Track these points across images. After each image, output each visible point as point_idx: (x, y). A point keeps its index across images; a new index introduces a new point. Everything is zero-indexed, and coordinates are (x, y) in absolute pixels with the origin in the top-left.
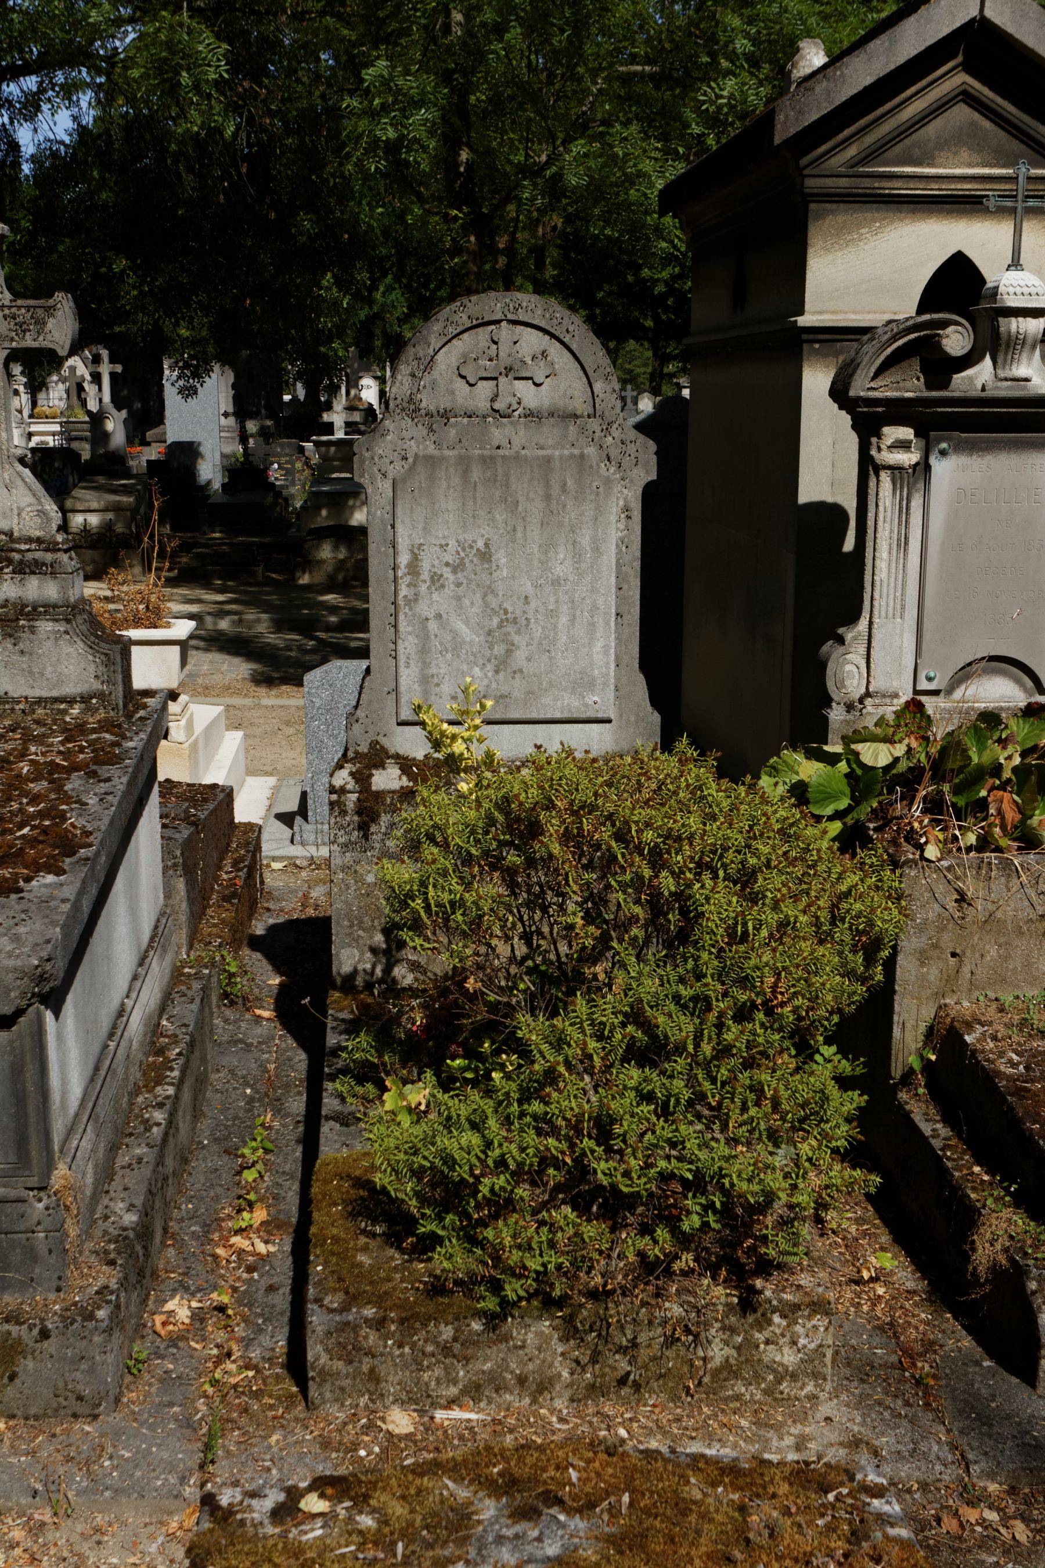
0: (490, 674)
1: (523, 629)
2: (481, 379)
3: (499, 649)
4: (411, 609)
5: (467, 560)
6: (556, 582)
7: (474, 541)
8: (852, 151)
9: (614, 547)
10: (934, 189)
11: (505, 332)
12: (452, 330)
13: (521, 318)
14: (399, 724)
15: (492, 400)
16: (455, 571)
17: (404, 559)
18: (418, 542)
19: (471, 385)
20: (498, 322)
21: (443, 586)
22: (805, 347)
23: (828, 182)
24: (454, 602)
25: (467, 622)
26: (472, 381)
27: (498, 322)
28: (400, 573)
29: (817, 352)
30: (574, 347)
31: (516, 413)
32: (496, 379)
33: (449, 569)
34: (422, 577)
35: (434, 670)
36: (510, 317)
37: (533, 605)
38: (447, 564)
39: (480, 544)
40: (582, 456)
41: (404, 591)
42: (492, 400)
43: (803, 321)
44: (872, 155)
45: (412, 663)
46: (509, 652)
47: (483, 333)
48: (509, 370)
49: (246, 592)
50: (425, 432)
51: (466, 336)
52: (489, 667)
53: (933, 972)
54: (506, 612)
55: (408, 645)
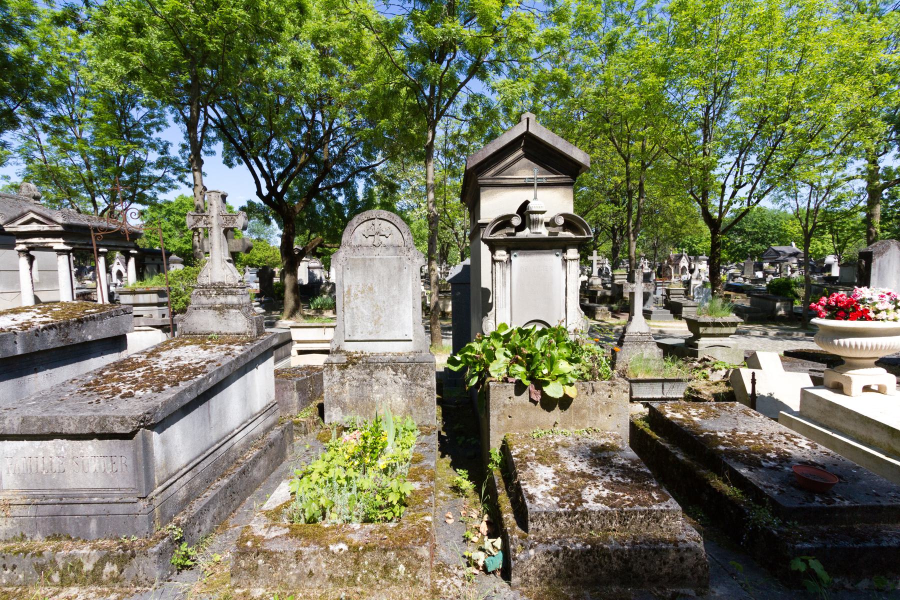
3: (376, 318)
6: (393, 297)
8: (492, 172)
10: (518, 182)
11: (376, 222)
17: (346, 289)
43: (479, 221)
44: (500, 172)
46: (379, 319)
47: (370, 222)
48: (377, 233)
49: (784, 329)
53: (503, 423)
55: (347, 316)
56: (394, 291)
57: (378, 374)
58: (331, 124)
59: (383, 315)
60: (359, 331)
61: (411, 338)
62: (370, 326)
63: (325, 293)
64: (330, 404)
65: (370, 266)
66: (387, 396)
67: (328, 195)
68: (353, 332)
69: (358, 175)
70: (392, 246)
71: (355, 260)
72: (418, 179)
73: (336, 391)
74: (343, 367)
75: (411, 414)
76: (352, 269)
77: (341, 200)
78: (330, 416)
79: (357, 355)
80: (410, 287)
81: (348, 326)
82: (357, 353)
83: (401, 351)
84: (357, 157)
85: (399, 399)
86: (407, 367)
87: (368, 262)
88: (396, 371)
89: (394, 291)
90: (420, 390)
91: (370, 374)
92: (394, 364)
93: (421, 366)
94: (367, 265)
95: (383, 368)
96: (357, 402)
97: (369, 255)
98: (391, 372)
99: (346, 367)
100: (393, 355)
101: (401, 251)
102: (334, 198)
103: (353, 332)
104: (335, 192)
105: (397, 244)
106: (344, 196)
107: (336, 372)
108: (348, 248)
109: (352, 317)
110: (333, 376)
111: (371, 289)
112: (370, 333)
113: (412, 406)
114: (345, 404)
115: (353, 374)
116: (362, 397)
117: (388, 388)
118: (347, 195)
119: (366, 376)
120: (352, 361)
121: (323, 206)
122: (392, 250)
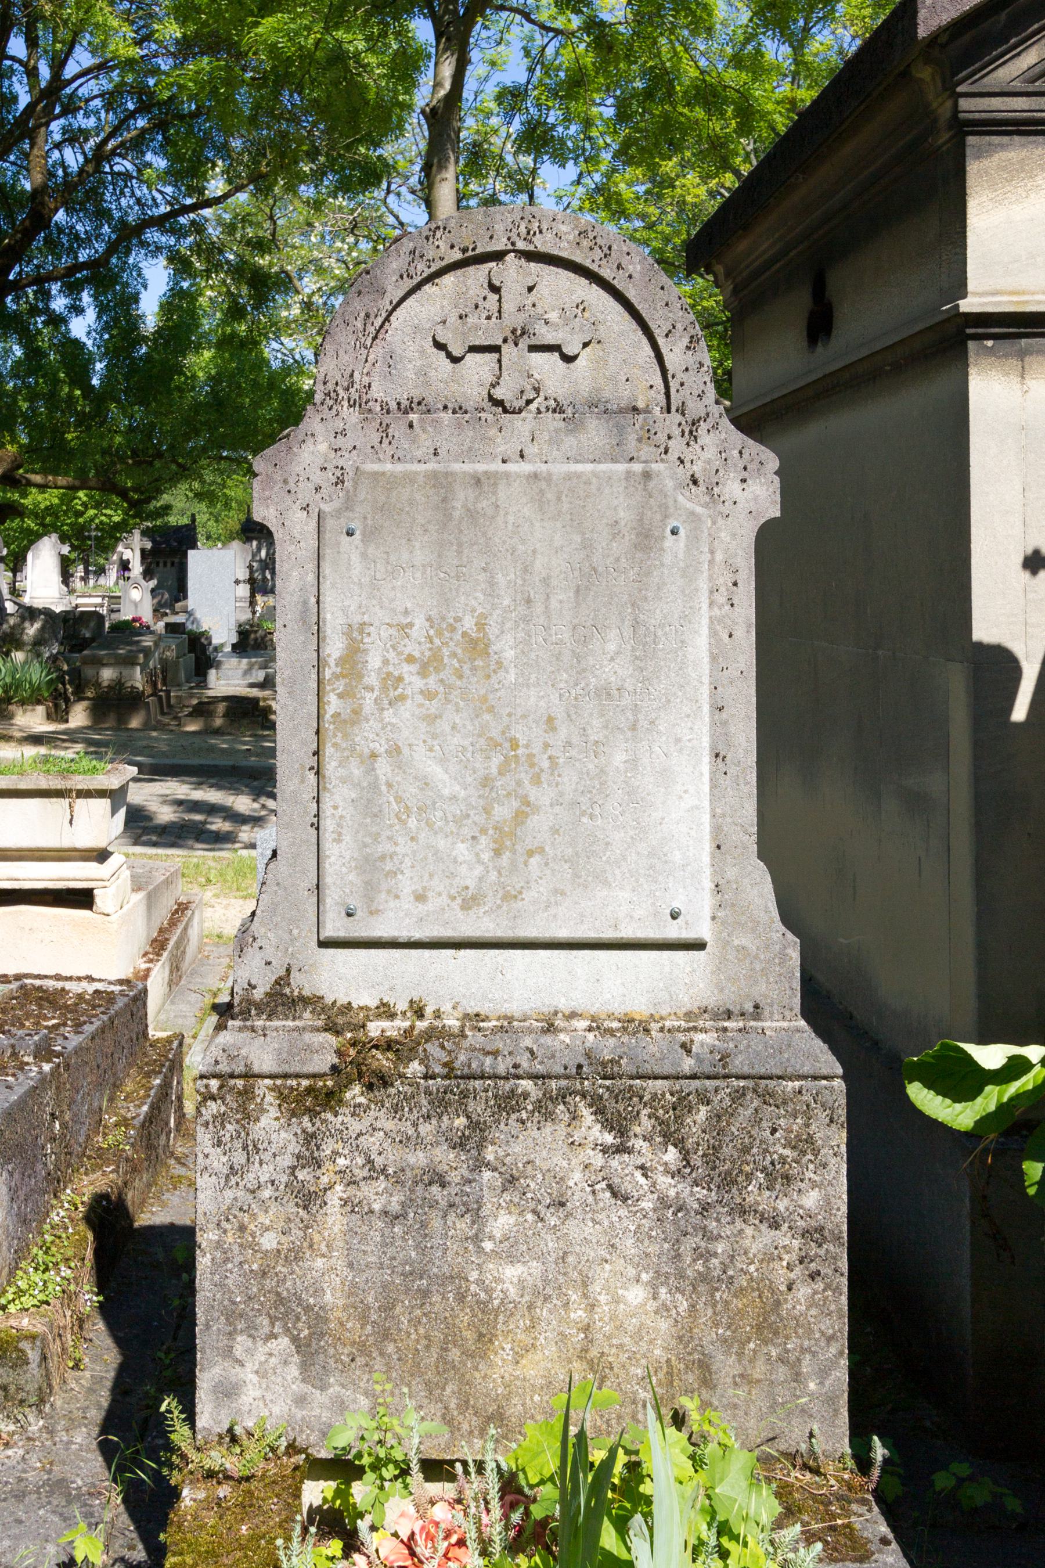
0: (486, 856)
1: (544, 777)
2: (474, 349)
3: (503, 812)
4: (346, 736)
5: (446, 652)
6: (605, 693)
7: (458, 619)
9: (705, 631)
11: (512, 273)
12: (422, 269)
13: (542, 249)
14: (323, 944)
15: (493, 386)
16: (423, 673)
17: (335, 648)
18: (357, 619)
19: (455, 360)
20: (498, 256)
21: (402, 698)
22: (971, 345)
23: (996, 103)
24: (423, 726)
25: (443, 761)
26: (456, 352)
27: (498, 256)
28: (328, 674)
29: (990, 352)
30: (631, 294)
31: (533, 407)
32: (495, 349)
33: (414, 668)
34: (366, 680)
35: (385, 847)
36: (521, 245)
37: (563, 732)
38: (410, 659)
39: (469, 623)
40: (647, 475)
41: (333, 704)
42: (493, 386)
43: (967, 305)
45: (347, 838)
46: (520, 817)
47: (477, 275)
48: (517, 335)
50: (375, 437)
51: (448, 279)
52: (483, 840)
54: (514, 744)
55: (339, 800)
56: (611, 661)
57: (519, 1143)
58: (58, 65)
59: (541, 796)
60: (407, 885)
61: (703, 931)
62: (469, 861)
63: (19, 645)
64: (232, 1315)
65: (472, 514)
66: (567, 1276)
67: (34, 311)
68: (370, 890)
69: (144, 244)
70: (598, 406)
71: (392, 483)
72: (321, 271)
73: (269, 1241)
74: (313, 1099)
75: (707, 1382)
76: (371, 534)
77: (82, 327)
78: (228, 1391)
79: (393, 1028)
80: (700, 645)
81: (339, 856)
82: (386, 1011)
83: (640, 1007)
84: (146, 184)
85: (636, 1295)
86: (682, 1105)
87: (462, 496)
88: (618, 1125)
89: (611, 661)
90: (757, 1240)
91: (471, 1140)
92: (608, 1085)
93: (767, 1097)
94: (456, 512)
95: (544, 1110)
96: (387, 1308)
97: (469, 454)
98: (592, 1129)
99: (330, 1099)
100: (596, 1026)
101: (648, 435)
102: (57, 321)
103: (370, 890)
104: (59, 304)
105: (624, 394)
106: (91, 314)
107: (271, 1125)
108: (351, 416)
109: (369, 805)
110: (252, 1149)
111: (477, 646)
112: (470, 902)
113: (708, 1336)
114: (318, 1318)
115: (372, 1142)
116: (419, 1281)
117: (574, 1229)
118: (102, 309)
119: (444, 1156)
120: (366, 1063)
121: (18, 351)
122: (596, 433)
